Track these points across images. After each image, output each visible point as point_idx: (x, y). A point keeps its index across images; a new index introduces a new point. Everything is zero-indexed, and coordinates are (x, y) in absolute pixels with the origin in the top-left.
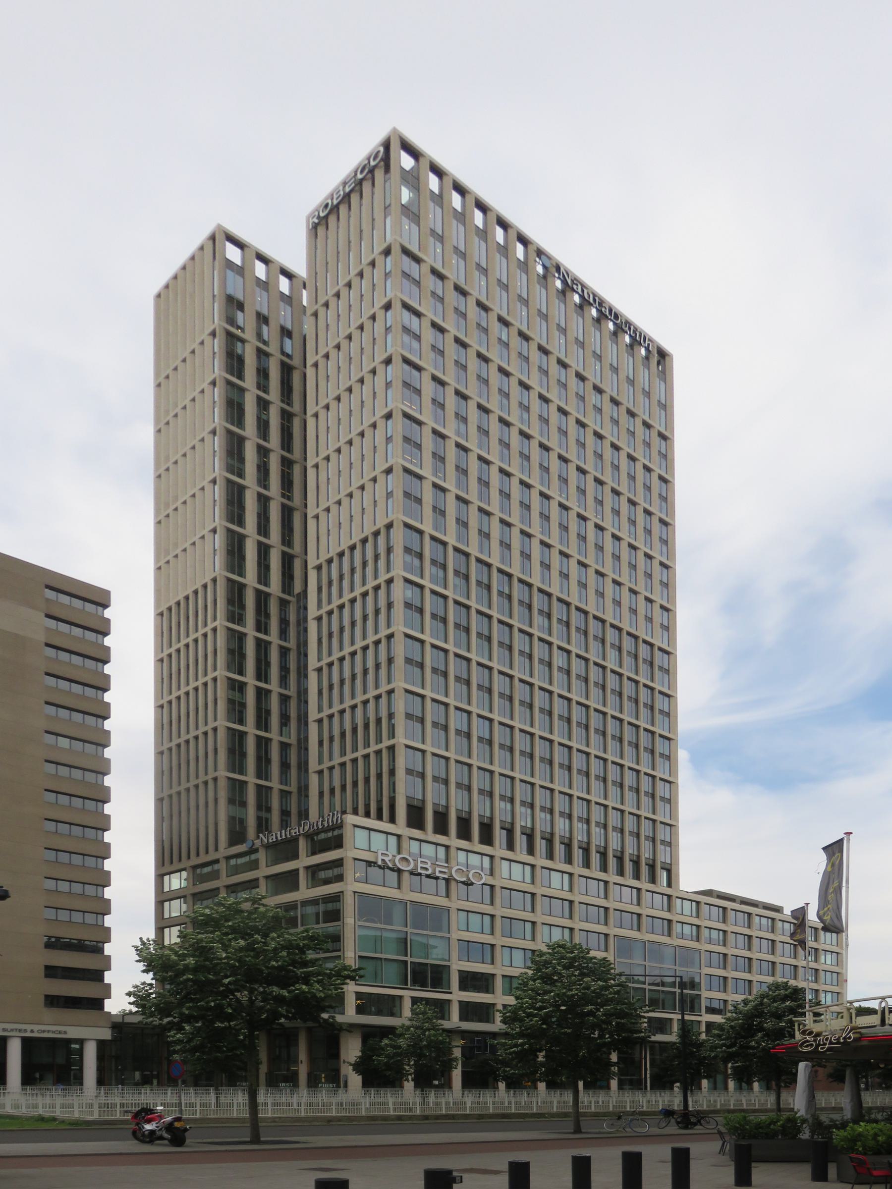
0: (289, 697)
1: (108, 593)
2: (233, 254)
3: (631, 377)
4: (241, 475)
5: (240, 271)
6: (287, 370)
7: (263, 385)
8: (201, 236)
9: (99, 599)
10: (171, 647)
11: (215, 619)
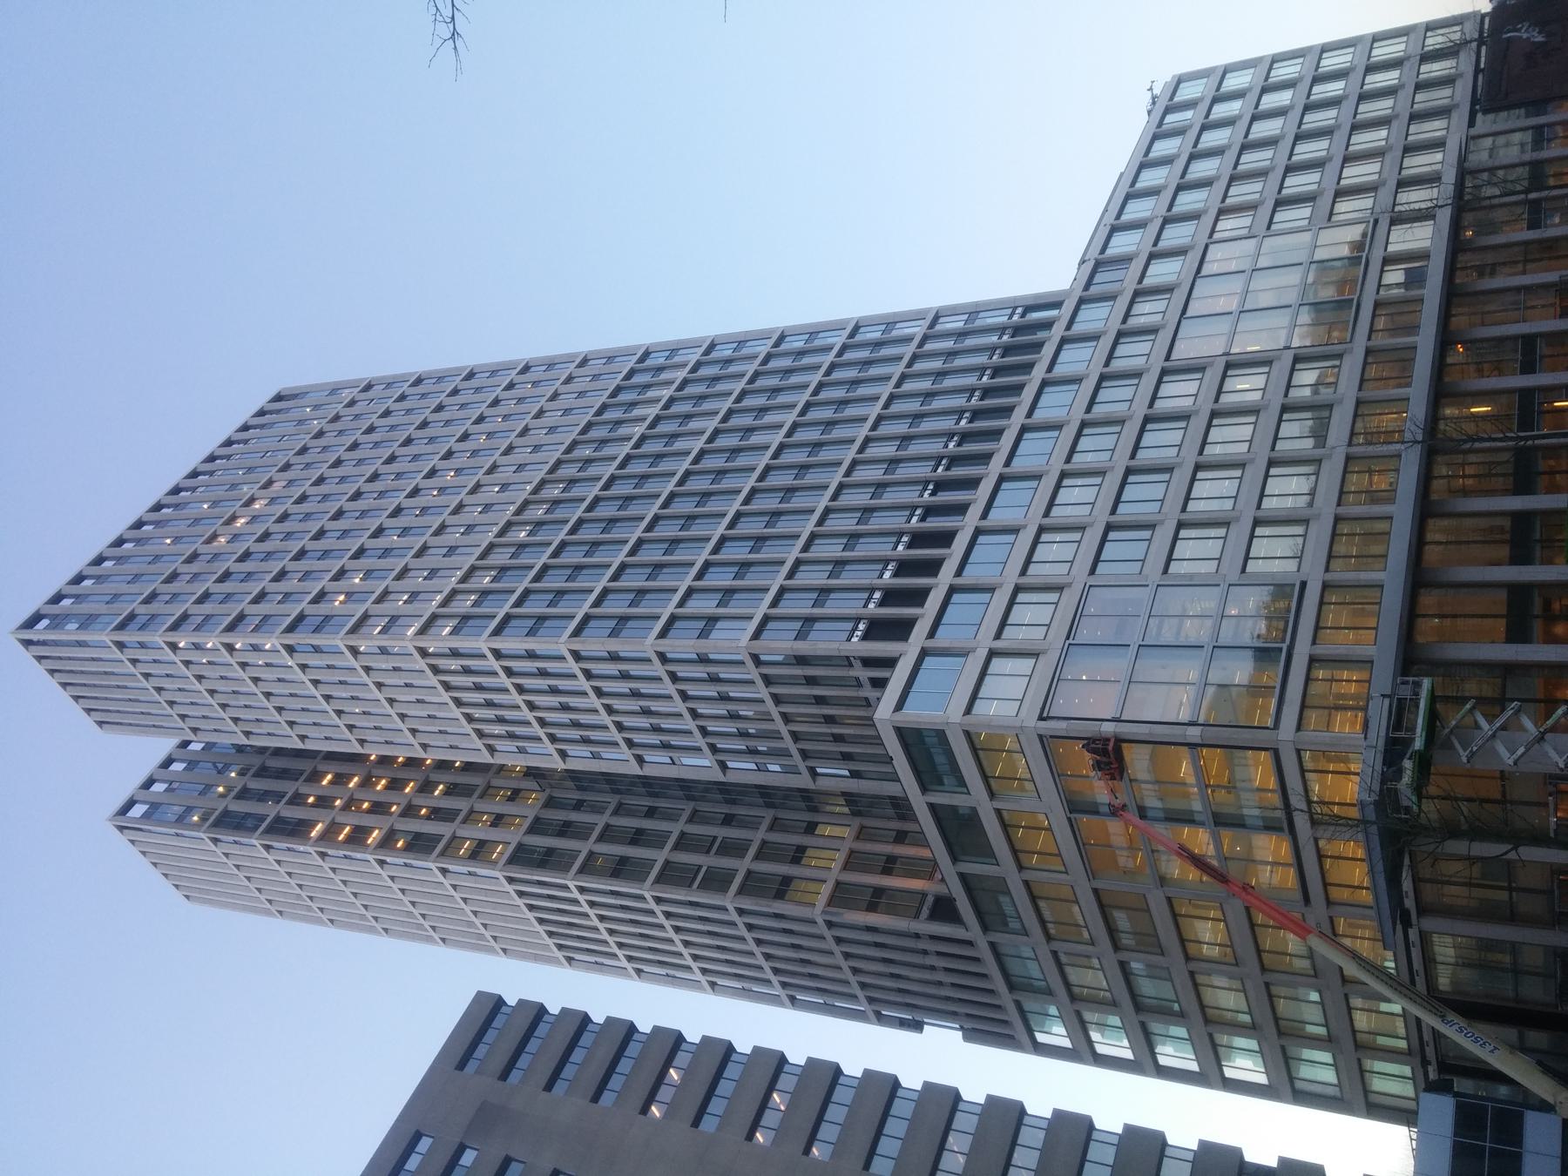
0: (695, 812)
1: (480, 995)
2: (138, 811)
3: (108, 598)
4: (262, 818)
5: (154, 806)
6: (263, 772)
7: (277, 797)
8: (121, 839)
9: (488, 1009)
10: (769, 981)
11: (566, 888)
